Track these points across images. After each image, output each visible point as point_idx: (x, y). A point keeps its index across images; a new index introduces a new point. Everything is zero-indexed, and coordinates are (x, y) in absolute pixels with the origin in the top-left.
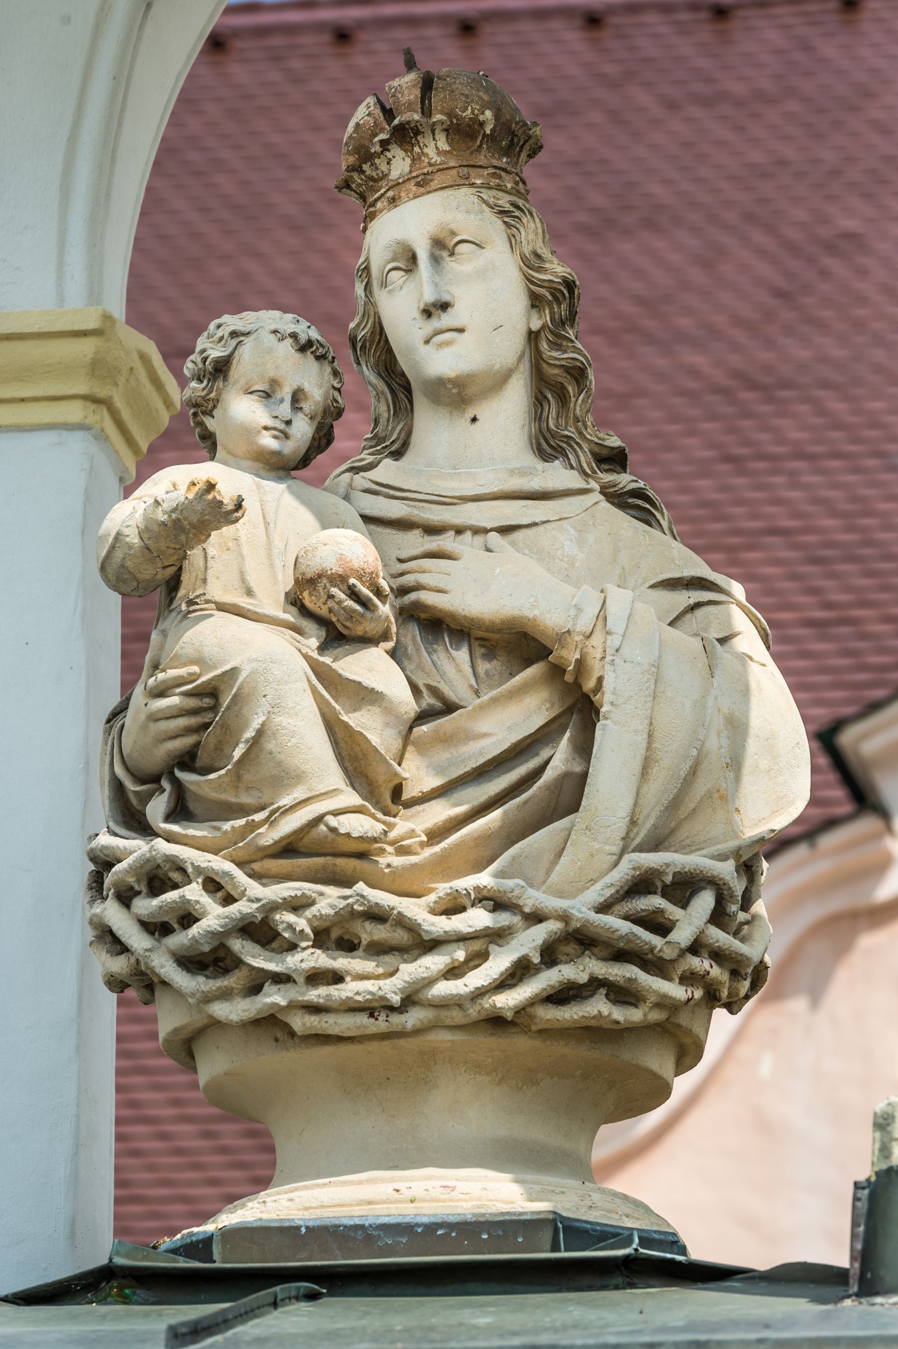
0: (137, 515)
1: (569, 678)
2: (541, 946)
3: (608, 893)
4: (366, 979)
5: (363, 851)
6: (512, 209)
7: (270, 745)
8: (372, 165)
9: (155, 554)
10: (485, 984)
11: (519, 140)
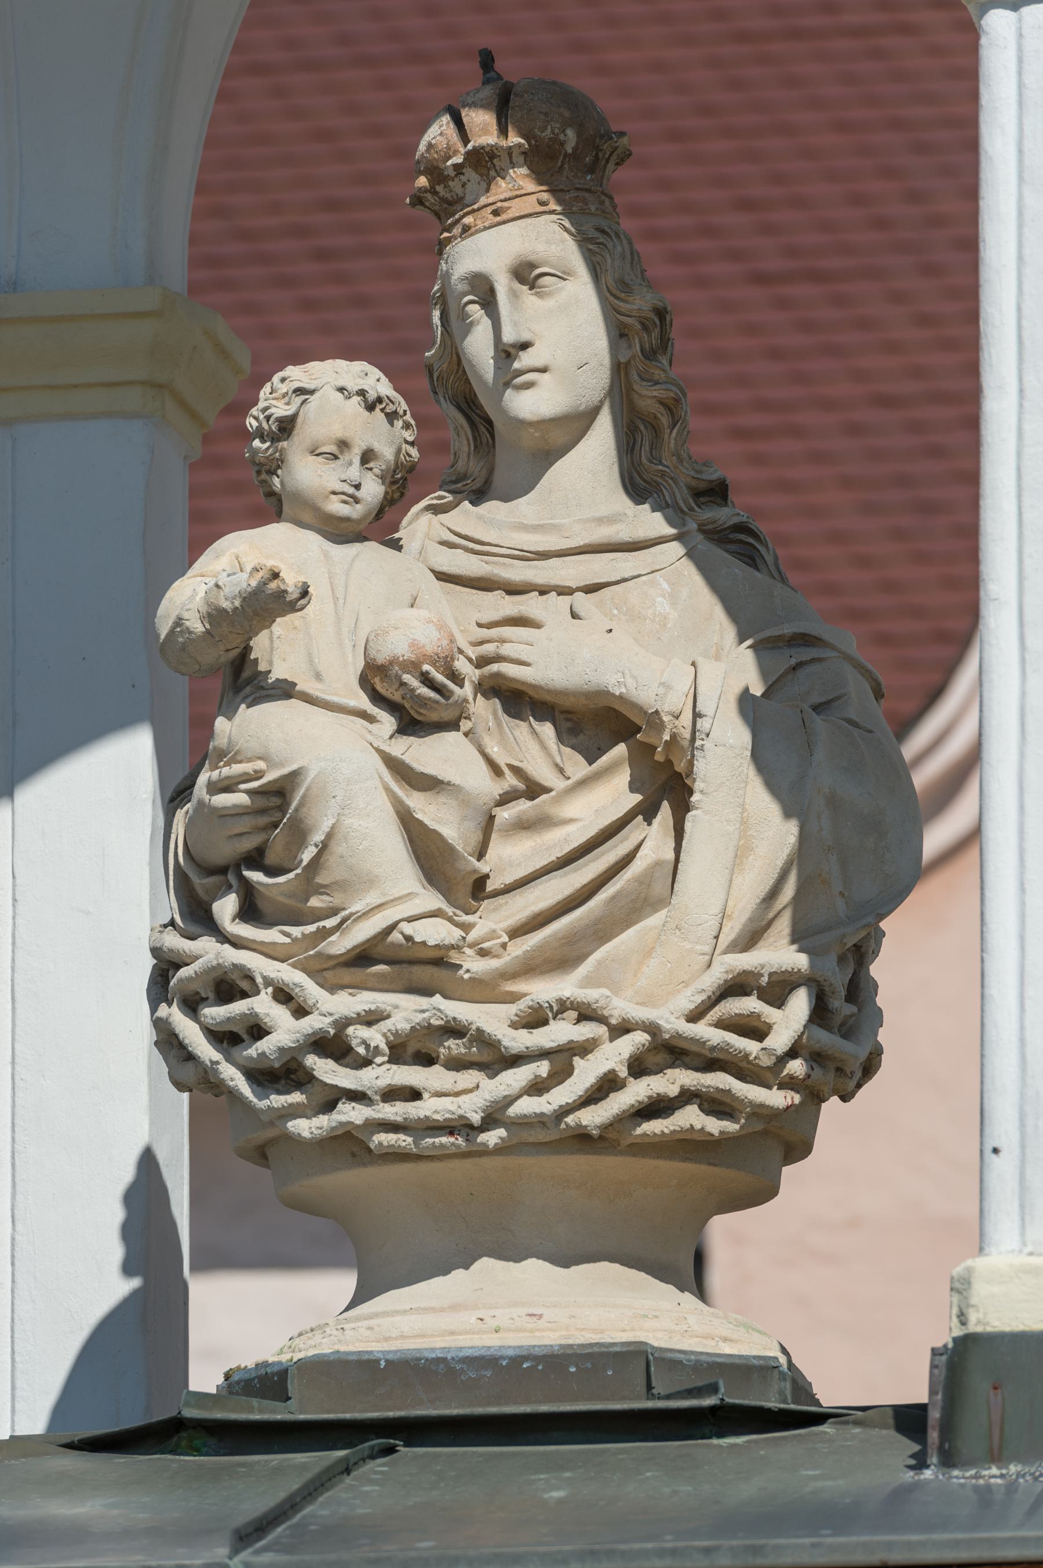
0: (198, 599)
1: (659, 757)
2: (628, 1060)
3: (699, 999)
4: (451, 1094)
5: (440, 960)
7: (338, 848)
8: (445, 187)
9: (217, 639)
10: (570, 1101)
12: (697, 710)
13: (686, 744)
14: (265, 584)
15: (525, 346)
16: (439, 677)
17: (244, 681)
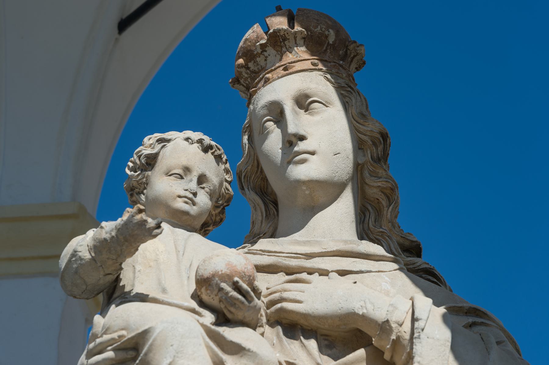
6: (346, 86)
8: (255, 62)
9: (99, 264)
11: (351, 53)
12: (415, 317)
13: (406, 342)
14: (133, 216)
15: (302, 138)
16: (245, 286)
17: (114, 293)
